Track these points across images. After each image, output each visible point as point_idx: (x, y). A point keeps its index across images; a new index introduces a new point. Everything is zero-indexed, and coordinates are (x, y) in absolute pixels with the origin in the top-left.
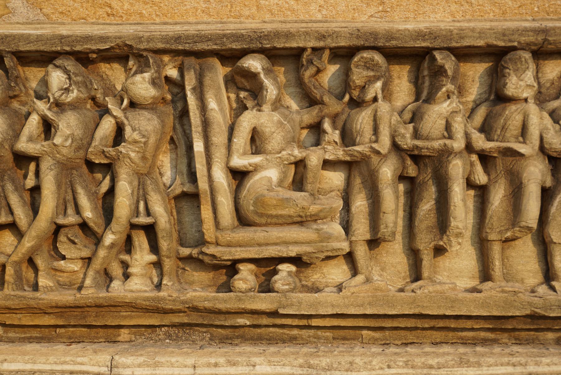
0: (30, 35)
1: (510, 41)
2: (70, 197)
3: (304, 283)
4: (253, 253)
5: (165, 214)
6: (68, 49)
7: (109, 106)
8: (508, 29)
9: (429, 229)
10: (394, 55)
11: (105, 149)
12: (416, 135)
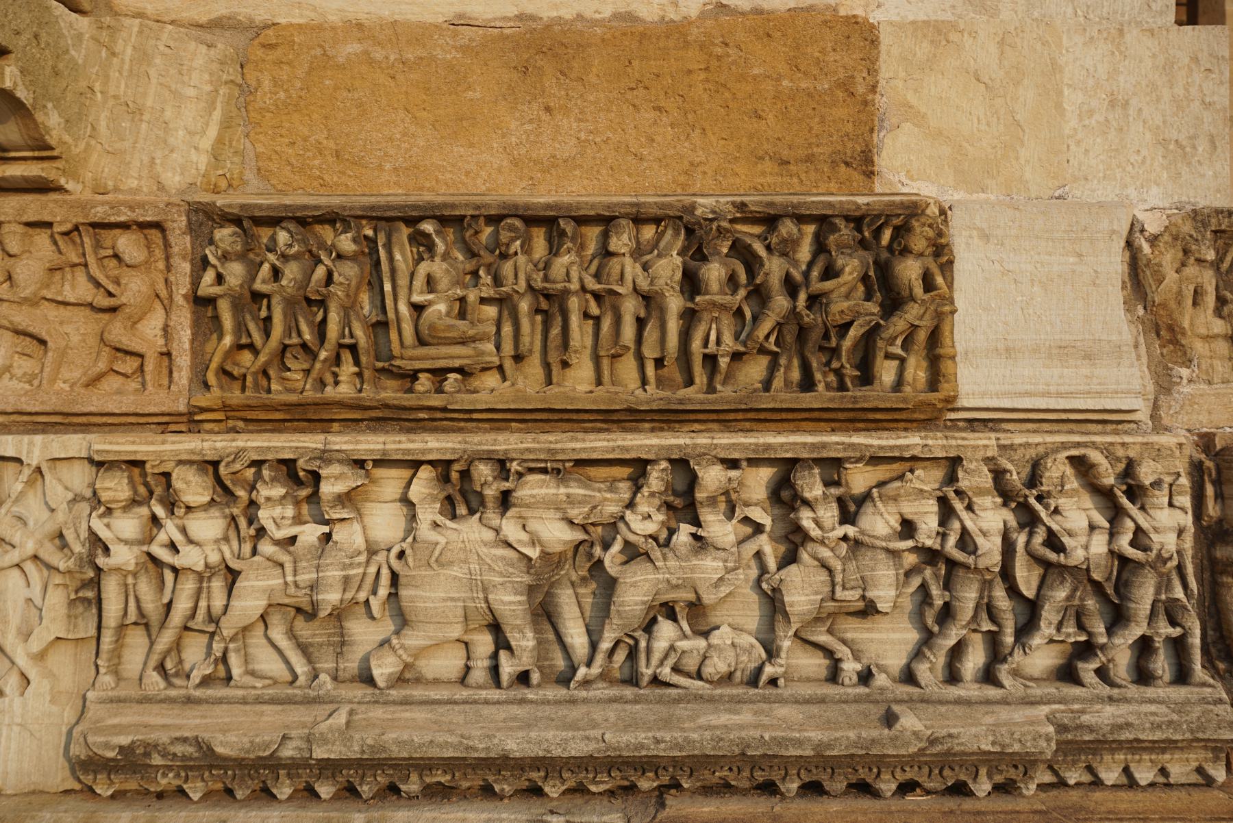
2: (293, 324)
9: (557, 348)
10: (532, 219)
12: (546, 279)
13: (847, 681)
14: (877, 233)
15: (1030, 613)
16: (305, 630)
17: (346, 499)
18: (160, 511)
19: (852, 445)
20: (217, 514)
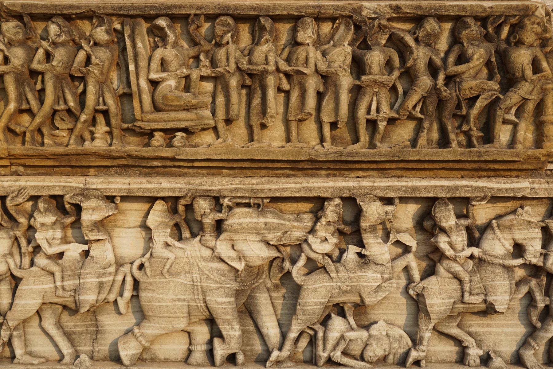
0: (38, 4)
1: (301, 12)
2: (61, 95)
3: (190, 143)
4: (161, 126)
5: (114, 104)
6: (59, 12)
7: (83, 45)
8: (300, 6)
10: (239, 18)
11: (81, 68)
12: (250, 62)
14: (498, 29)
16: (68, 321)
17: (100, 225)
19: (478, 188)
20: (5, 235)
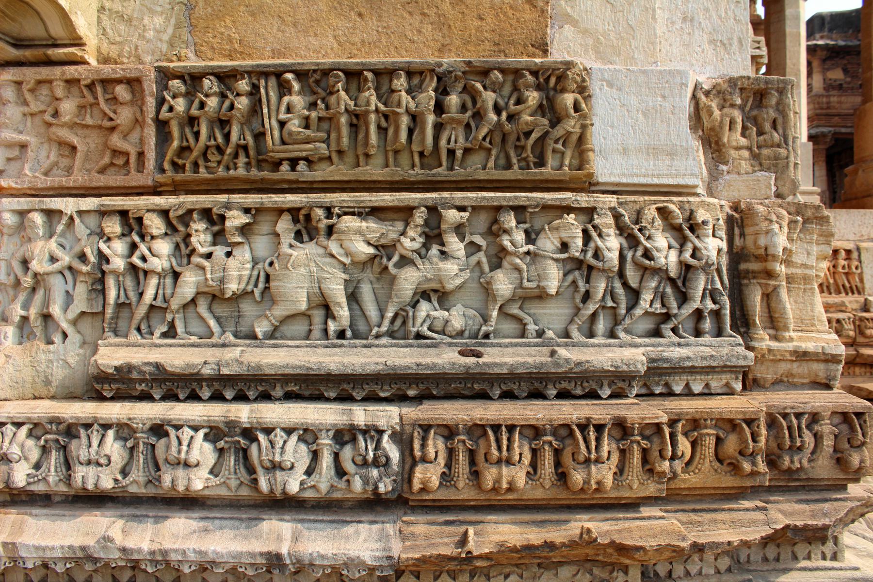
12: (355, 105)
13: (530, 335)
14: (547, 80)
15: (634, 295)
18: (137, 239)
